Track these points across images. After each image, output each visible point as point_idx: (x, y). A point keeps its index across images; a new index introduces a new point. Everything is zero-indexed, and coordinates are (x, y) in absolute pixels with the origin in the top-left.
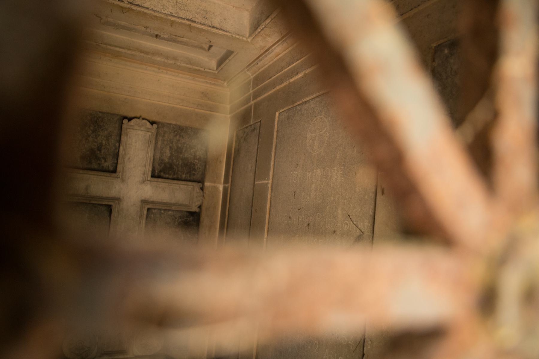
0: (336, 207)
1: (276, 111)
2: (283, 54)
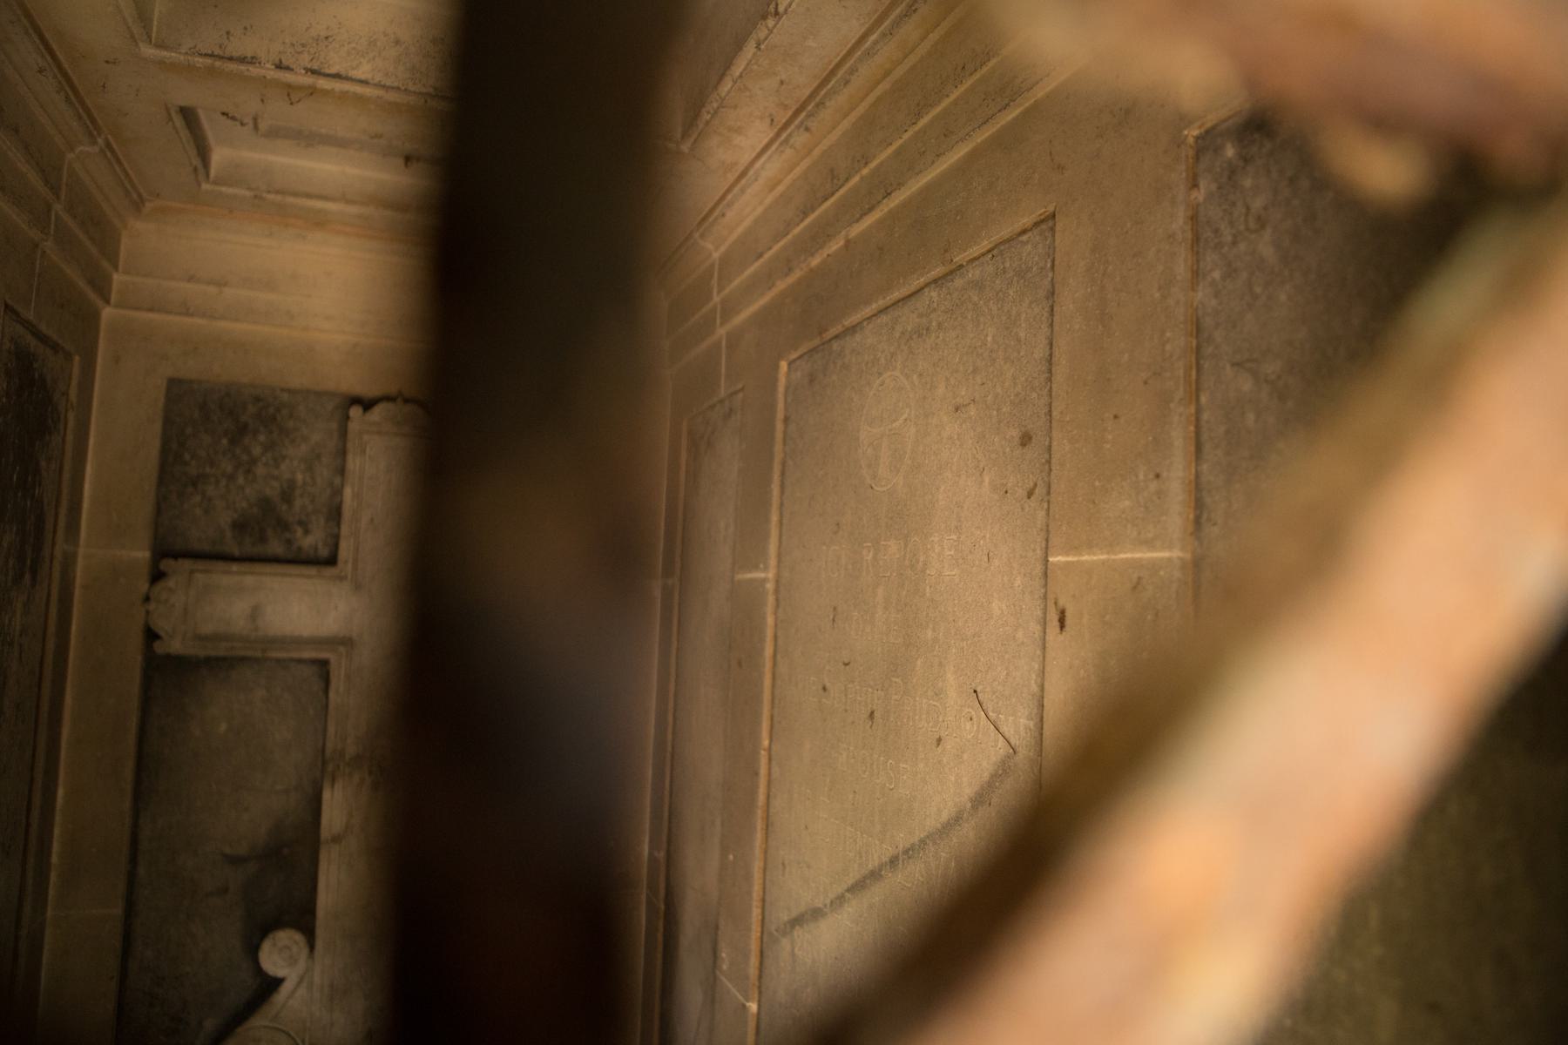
0: (941, 664)
1: (780, 357)
2: (788, 180)
